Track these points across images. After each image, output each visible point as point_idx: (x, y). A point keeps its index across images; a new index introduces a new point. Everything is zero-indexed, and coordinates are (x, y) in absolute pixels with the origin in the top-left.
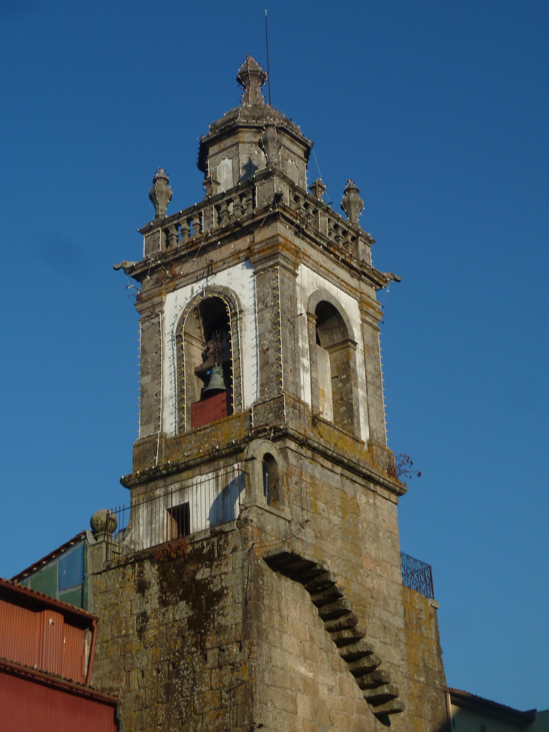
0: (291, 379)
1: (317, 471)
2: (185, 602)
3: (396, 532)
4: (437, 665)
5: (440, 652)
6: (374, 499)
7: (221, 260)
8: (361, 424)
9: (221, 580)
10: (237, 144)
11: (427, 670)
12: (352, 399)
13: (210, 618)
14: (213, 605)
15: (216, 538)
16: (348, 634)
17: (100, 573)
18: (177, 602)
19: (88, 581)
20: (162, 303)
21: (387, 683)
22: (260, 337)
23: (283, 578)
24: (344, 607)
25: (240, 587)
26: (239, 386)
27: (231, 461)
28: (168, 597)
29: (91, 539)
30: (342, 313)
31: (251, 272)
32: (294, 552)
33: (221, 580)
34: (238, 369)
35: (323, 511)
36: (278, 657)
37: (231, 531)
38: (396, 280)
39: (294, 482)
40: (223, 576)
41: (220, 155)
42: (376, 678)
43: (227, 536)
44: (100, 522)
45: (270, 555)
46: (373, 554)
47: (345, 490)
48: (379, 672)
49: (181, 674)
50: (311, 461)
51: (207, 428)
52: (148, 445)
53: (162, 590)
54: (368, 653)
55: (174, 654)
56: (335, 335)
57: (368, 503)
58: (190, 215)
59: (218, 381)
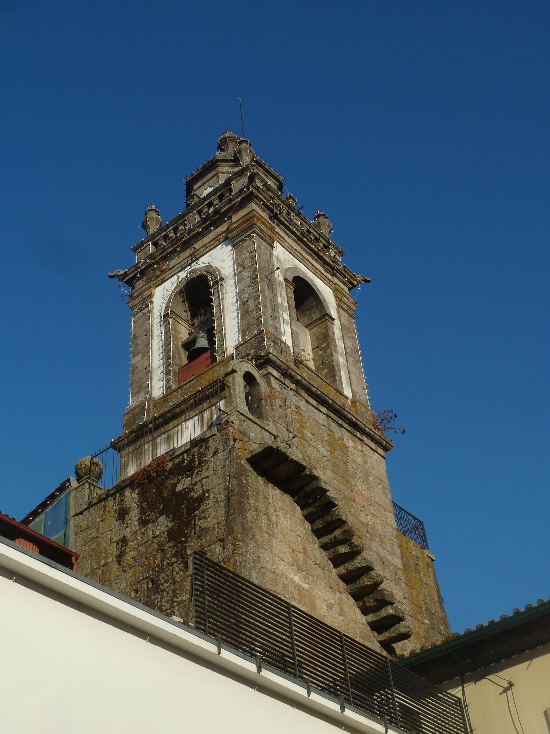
0: (271, 322)
1: (303, 404)
2: (165, 516)
3: (386, 481)
4: (440, 611)
5: (441, 601)
6: (362, 447)
7: (203, 246)
8: (344, 385)
9: (202, 485)
10: (217, 174)
11: (431, 616)
12: (333, 361)
13: (191, 524)
14: (195, 510)
15: (197, 448)
16: (345, 548)
17: (81, 513)
18: (157, 518)
19: (71, 523)
20: (151, 296)
21: (392, 604)
22: (240, 293)
23: (270, 485)
24: (338, 516)
25: (222, 486)
26: (222, 338)
27: (213, 401)
28: (148, 516)
29: (74, 484)
30: (318, 293)
31: (230, 247)
32: (279, 449)
33: (202, 485)
34: (220, 325)
35: (311, 439)
36: (267, 559)
37: (211, 437)
38: (366, 281)
39: (278, 405)
40: (204, 481)
41: (203, 187)
42: (379, 598)
43: (208, 442)
44: (84, 466)
45: (254, 453)
46: (365, 493)
47: (332, 429)
48: (382, 590)
49: (160, 588)
50: (295, 393)
51: (192, 380)
52: (137, 410)
53: (142, 511)
54: (368, 569)
55: (153, 570)
56: (313, 314)
57: (355, 447)
58: (176, 225)
59: (202, 342)
